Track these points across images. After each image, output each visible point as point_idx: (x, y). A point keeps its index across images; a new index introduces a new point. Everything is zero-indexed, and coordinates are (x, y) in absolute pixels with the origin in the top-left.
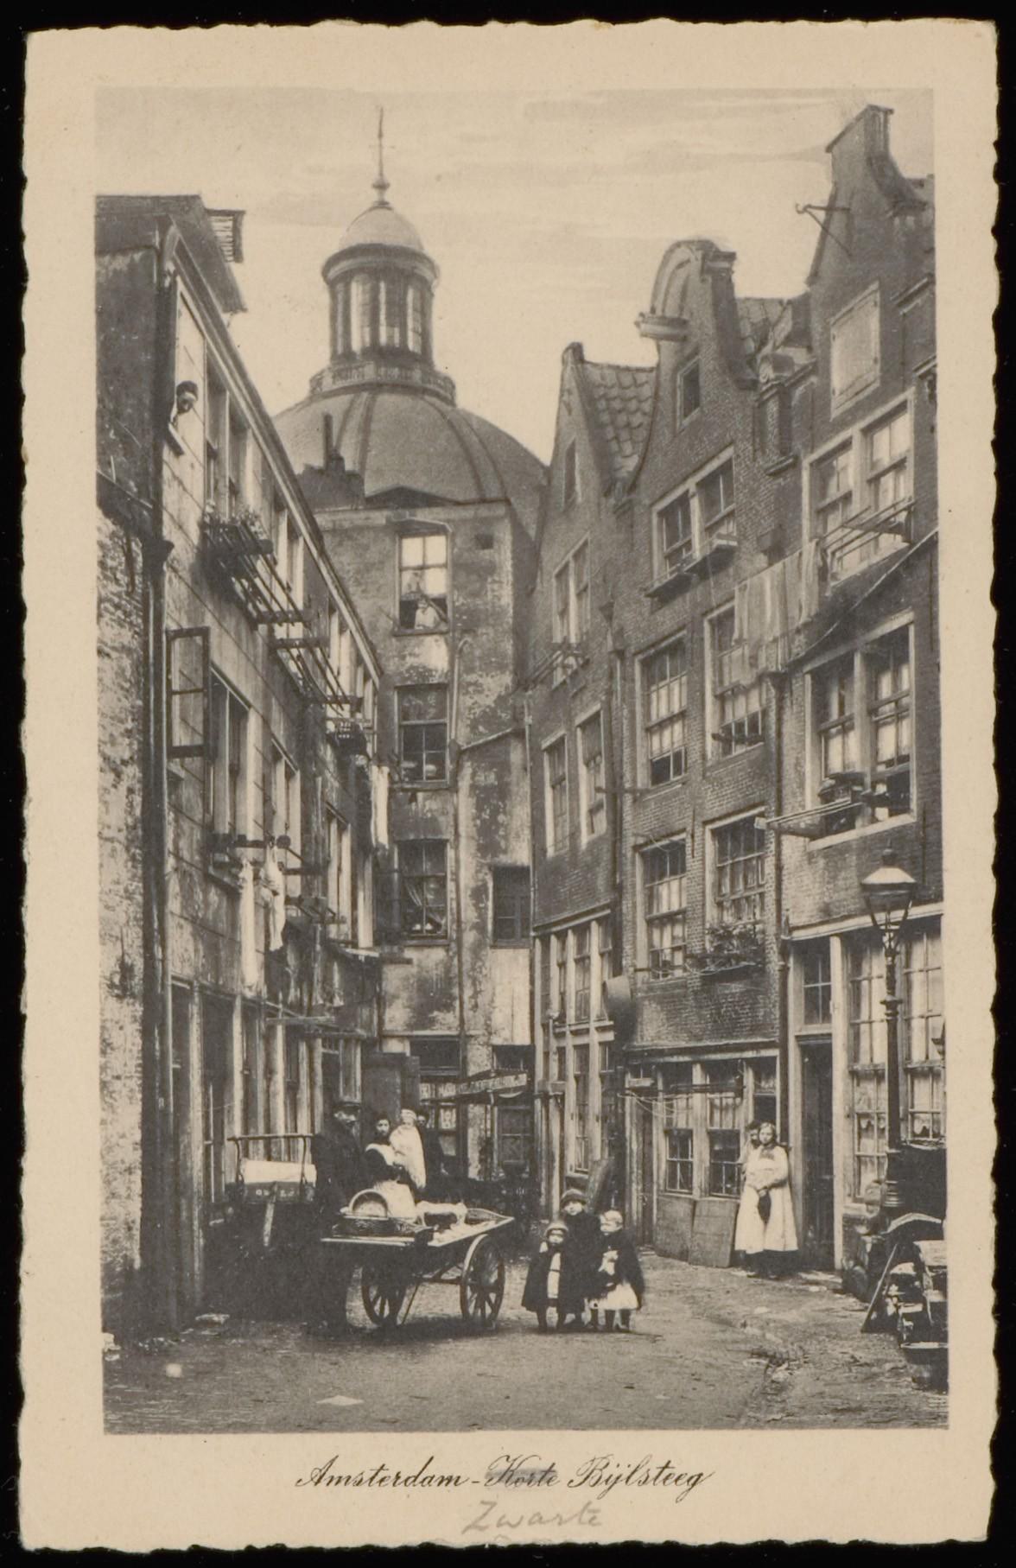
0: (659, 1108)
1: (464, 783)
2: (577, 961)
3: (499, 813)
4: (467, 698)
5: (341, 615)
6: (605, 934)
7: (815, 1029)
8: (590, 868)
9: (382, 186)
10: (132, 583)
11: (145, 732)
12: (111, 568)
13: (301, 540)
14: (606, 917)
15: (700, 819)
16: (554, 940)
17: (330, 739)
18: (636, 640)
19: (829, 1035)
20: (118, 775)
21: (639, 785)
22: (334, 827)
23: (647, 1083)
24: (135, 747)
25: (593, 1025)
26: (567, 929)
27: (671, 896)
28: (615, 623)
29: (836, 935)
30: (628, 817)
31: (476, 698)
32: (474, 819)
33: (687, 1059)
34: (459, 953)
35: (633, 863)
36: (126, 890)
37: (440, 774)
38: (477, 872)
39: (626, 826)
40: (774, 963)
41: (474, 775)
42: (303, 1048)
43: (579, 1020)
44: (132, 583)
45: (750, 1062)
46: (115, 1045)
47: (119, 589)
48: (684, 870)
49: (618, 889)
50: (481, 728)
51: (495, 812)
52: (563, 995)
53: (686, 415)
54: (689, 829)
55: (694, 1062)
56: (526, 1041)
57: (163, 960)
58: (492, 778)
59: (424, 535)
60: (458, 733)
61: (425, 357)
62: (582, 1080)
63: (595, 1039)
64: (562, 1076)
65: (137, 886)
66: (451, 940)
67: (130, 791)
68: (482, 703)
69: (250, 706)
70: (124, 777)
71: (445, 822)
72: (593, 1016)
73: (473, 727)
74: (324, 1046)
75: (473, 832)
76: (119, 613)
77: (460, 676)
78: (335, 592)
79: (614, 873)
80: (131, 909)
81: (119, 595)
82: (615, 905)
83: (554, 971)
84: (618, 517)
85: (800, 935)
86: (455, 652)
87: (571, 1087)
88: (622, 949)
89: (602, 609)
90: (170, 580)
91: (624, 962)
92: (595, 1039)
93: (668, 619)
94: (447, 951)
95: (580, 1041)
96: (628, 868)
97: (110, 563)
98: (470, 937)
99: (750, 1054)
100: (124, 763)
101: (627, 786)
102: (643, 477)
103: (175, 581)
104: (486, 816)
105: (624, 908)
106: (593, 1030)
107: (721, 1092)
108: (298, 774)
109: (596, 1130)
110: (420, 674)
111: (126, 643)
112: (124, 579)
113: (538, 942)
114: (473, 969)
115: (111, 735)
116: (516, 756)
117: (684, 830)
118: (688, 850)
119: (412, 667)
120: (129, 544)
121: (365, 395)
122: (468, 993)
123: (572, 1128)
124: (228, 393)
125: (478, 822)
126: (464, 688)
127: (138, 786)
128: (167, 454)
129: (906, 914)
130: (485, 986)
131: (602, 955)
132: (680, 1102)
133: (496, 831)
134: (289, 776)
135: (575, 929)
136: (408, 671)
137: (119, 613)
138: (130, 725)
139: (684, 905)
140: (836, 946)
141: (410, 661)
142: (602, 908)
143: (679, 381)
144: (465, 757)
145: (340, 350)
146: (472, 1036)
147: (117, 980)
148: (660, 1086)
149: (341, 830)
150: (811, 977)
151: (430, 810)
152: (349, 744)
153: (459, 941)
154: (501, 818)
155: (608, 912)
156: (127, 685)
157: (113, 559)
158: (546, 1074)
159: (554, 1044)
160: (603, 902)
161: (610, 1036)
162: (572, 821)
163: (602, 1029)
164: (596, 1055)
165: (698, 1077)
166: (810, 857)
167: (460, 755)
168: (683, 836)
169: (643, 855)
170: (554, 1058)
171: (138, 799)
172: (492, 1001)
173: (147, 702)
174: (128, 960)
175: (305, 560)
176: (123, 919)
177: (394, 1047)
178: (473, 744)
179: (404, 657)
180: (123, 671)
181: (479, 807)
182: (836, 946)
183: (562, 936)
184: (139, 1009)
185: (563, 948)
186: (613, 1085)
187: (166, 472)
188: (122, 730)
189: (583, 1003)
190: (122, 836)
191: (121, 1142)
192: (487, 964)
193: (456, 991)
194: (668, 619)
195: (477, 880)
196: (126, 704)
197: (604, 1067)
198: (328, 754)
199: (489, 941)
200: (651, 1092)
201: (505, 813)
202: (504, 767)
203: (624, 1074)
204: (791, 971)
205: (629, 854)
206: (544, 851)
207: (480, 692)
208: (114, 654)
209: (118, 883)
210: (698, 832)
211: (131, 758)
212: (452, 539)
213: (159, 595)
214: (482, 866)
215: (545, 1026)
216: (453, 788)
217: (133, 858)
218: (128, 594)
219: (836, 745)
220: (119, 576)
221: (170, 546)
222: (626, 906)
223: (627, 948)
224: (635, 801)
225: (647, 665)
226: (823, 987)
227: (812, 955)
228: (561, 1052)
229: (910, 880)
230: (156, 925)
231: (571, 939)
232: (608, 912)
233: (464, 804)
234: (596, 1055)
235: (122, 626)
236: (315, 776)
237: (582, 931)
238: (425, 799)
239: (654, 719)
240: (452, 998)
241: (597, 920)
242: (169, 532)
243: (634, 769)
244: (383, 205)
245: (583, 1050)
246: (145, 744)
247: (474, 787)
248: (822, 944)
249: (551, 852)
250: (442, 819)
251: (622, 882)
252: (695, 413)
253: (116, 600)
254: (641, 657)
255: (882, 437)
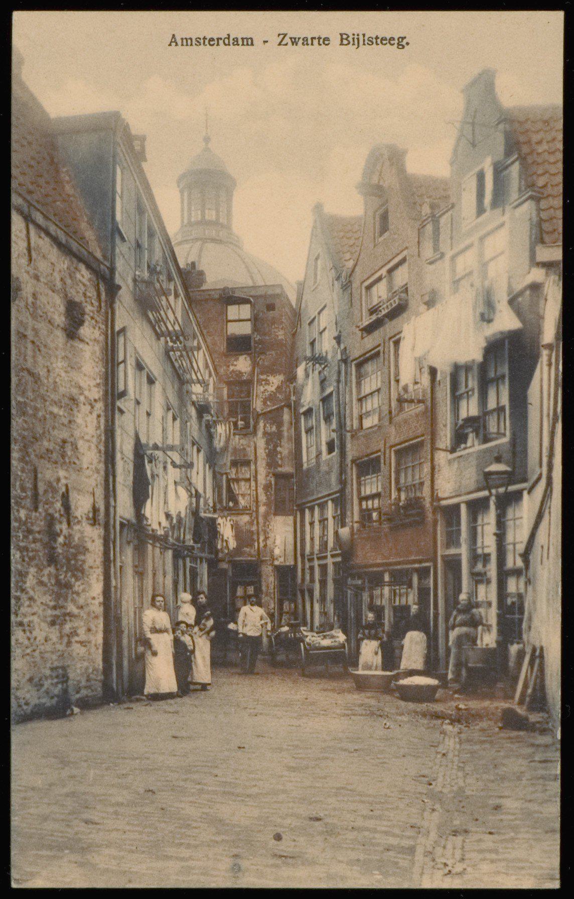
0: (366, 596)
1: (260, 433)
2: (320, 521)
3: (277, 446)
4: (262, 387)
5: (198, 340)
6: (336, 506)
7: (452, 551)
8: (328, 473)
9: (207, 140)
10: (100, 306)
11: (106, 384)
12: (89, 297)
13: (180, 299)
14: (337, 498)
15: (388, 445)
16: (307, 511)
17: (193, 403)
18: (356, 353)
19: (460, 555)
20: (92, 407)
21: (355, 428)
22: (195, 448)
23: (360, 582)
24: (101, 393)
25: (329, 554)
26: (314, 505)
27: (372, 486)
28: (342, 347)
29: (463, 502)
30: (349, 446)
31: (267, 387)
32: (265, 449)
33: (381, 569)
34: (257, 518)
35: (352, 469)
36: (96, 468)
37: (247, 426)
38: (267, 476)
39: (347, 450)
40: (430, 516)
41: (265, 426)
42: (181, 562)
43: (320, 551)
44: (100, 306)
45: (417, 570)
46: (90, 550)
47: (93, 308)
48: (379, 470)
49: (343, 483)
50: (268, 403)
51: (275, 446)
52: (312, 539)
53: (380, 236)
54: (382, 450)
55: (385, 571)
56: (292, 563)
57: (115, 507)
58: (274, 428)
59: (239, 304)
60: (258, 405)
61: (228, 227)
62: (323, 583)
63: (330, 561)
64: (312, 580)
65: (102, 466)
66: (253, 511)
67: (99, 416)
68: (269, 390)
69: (156, 379)
70: (95, 409)
71: (250, 451)
72: (329, 549)
73: (264, 403)
74: (191, 562)
75: (264, 455)
76: (93, 321)
77: (257, 376)
78: (196, 329)
79: (341, 474)
80: (99, 479)
81: (93, 312)
82: (342, 491)
83: (308, 527)
84: (344, 291)
85: (444, 503)
86: (254, 364)
87: (317, 586)
88: (345, 514)
89: (335, 338)
90: (119, 308)
91: (347, 521)
92: (330, 561)
93: (370, 342)
94: (251, 517)
95: (322, 562)
96: (349, 471)
97: (89, 294)
98: (262, 509)
99: (417, 566)
100: (95, 400)
101: (348, 429)
102: (357, 269)
103: (121, 307)
104: (271, 447)
105: (347, 491)
106: (329, 556)
107: (400, 585)
108: (179, 419)
109: (331, 608)
110: (237, 375)
111: (97, 337)
112: (96, 304)
113: (298, 513)
114: (264, 526)
115: (89, 386)
116: (286, 417)
117: (380, 451)
118: (382, 461)
119: (233, 371)
120: (98, 285)
121: (199, 243)
122: (262, 538)
123: (317, 607)
124: (147, 215)
125: (267, 451)
126: (259, 381)
127: (102, 414)
128: (118, 240)
129: (507, 489)
130: (271, 535)
131: (334, 517)
132: (377, 592)
133: (276, 456)
134: (174, 419)
135: (319, 505)
136: (231, 373)
137: (93, 321)
138: (98, 381)
139: (380, 490)
140: (463, 509)
141: (232, 368)
142: (336, 493)
143: (378, 219)
144: (260, 417)
145: (186, 221)
146: (264, 561)
147: (91, 515)
148: (367, 584)
149: (199, 451)
150: (449, 523)
151: (242, 445)
152: (202, 410)
153: (257, 511)
154: (279, 449)
155: (338, 495)
156: (97, 360)
157: (90, 292)
158: (303, 580)
159: (307, 566)
160: (335, 490)
161: (339, 559)
162: (317, 448)
163: (333, 556)
164: (331, 569)
165: (387, 578)
166: (450, 462)
167: (258, 415)
168: (379, 454)
169: (357, 465)
170: (307, 572)
171: (102, 420)
172: (275, 543)
173: (107, 369)
174: (97, 506)
175: (182, 310)
176: (94, 483)
177: (224, 566)
178: (265, 411)
179: (228, 366)
180: (95, 352)
181: (267, 443)
182: (463, 509)
183: (312, 509)
184: (101, 531)
185: (312, 516)
186: (340, 584)
187: (117, 250)
188: (95, 384)
189: (324, 545)
190: (94, 440)
191: (93, 602)
192: (272, 524)
193: (255, 537)
194: (370, 342)
195: (267, 481)
196: (97, 370)
197: (335, 575)
198: (193, 412)
199: (272, 512)
200: (362, 589)
201: (281, 447)
202: (280, 424)
203: (347, 578)
204: (439, 523)
205: (349, 465)
206: (302, 466)
207: (269, 384)
208: (91, 343)
209: (91, 464)
210: (387, 452)
211: (99, 399)
212: (253, 306)
213: (113, 313)
214: (269, 473)
215: (303, 556)
216: (255, 432)
217: (100, 452)
218: (98, 312)
219: (463, 404)
220: (93, 301)
221: (119, 287)
222: (348, 490)
223: (349, 513)
224: (352, 436)
225: (360, 366)
226: (456, 530)
227: (451, 513)
228: (312, 568)
229: (509, 469)
230: (111, 489)
231: (317, 509)
232: (338, 495)
233: (261, 442)
234: (331, 569)
235: (94, 328)
236: (186, 422)
237: (322, 506)
238: (239, 439)
239: (363, 394)
240: (253, 540)
241: (333, 500)
242: (118, 280)
243: (352, 420)
244: (207, 149)
245: (324, 568)
246: (106, 392)
247: (265, 433)
248: (457, 507)
249: (305, 466)
250: (248, 449)
251: (345, 479)
252: (386, 234)
253: (91, 314)
254: (355, 362)
255: (489, 242)
